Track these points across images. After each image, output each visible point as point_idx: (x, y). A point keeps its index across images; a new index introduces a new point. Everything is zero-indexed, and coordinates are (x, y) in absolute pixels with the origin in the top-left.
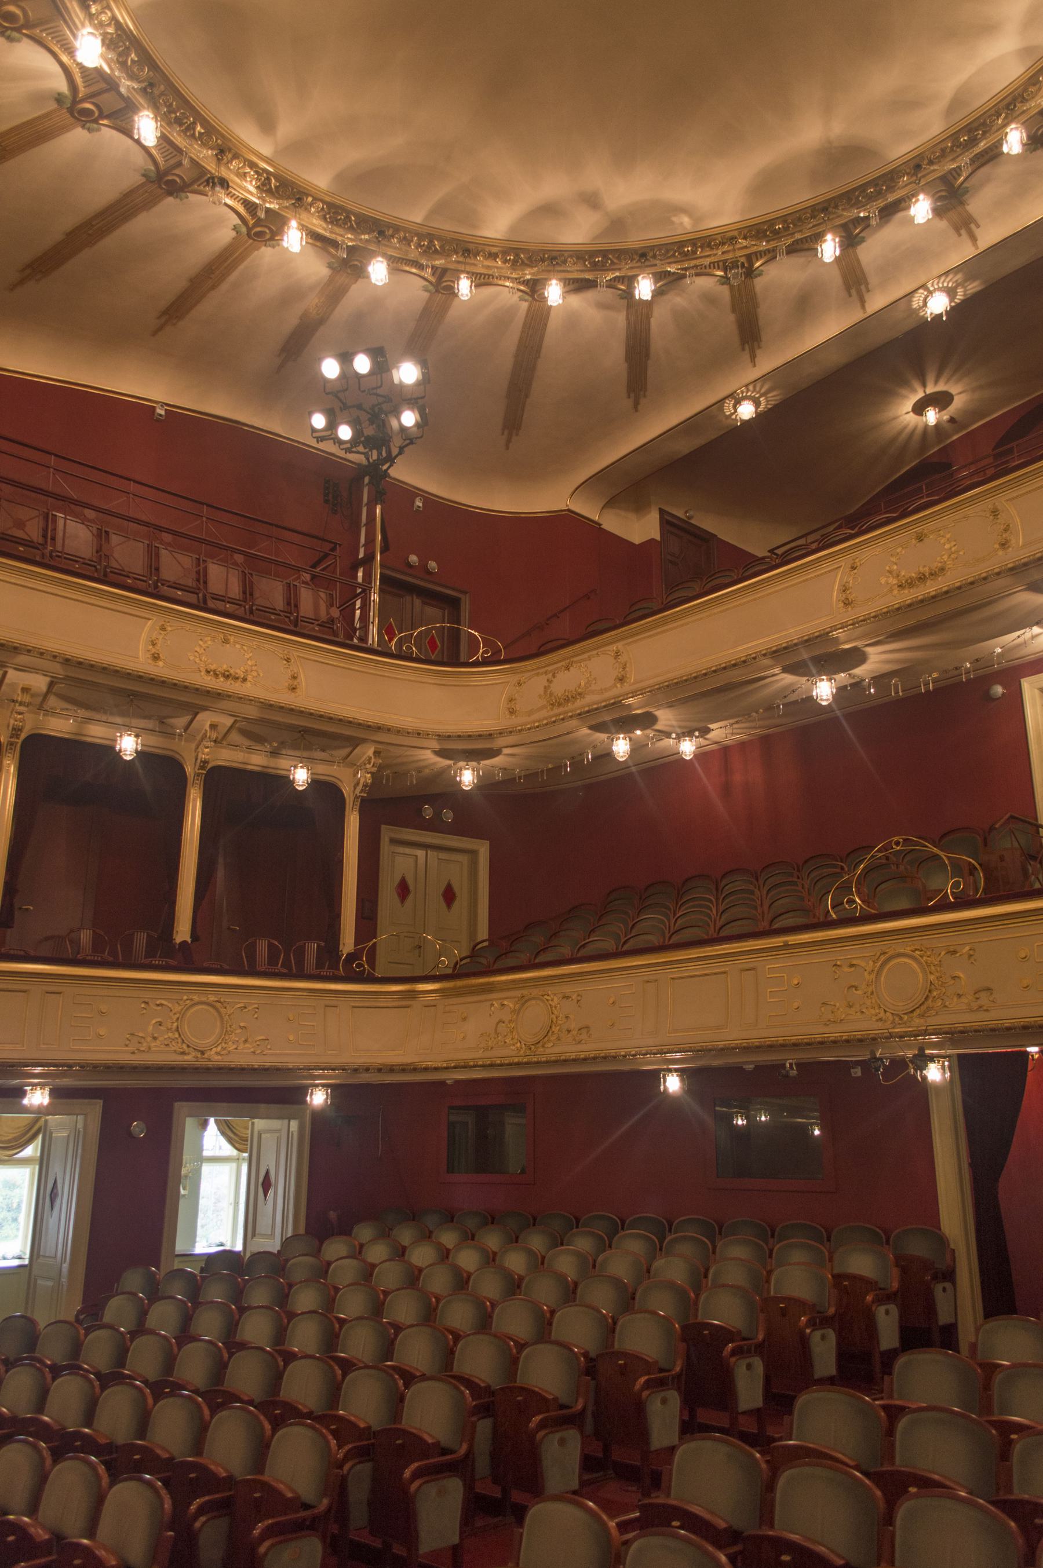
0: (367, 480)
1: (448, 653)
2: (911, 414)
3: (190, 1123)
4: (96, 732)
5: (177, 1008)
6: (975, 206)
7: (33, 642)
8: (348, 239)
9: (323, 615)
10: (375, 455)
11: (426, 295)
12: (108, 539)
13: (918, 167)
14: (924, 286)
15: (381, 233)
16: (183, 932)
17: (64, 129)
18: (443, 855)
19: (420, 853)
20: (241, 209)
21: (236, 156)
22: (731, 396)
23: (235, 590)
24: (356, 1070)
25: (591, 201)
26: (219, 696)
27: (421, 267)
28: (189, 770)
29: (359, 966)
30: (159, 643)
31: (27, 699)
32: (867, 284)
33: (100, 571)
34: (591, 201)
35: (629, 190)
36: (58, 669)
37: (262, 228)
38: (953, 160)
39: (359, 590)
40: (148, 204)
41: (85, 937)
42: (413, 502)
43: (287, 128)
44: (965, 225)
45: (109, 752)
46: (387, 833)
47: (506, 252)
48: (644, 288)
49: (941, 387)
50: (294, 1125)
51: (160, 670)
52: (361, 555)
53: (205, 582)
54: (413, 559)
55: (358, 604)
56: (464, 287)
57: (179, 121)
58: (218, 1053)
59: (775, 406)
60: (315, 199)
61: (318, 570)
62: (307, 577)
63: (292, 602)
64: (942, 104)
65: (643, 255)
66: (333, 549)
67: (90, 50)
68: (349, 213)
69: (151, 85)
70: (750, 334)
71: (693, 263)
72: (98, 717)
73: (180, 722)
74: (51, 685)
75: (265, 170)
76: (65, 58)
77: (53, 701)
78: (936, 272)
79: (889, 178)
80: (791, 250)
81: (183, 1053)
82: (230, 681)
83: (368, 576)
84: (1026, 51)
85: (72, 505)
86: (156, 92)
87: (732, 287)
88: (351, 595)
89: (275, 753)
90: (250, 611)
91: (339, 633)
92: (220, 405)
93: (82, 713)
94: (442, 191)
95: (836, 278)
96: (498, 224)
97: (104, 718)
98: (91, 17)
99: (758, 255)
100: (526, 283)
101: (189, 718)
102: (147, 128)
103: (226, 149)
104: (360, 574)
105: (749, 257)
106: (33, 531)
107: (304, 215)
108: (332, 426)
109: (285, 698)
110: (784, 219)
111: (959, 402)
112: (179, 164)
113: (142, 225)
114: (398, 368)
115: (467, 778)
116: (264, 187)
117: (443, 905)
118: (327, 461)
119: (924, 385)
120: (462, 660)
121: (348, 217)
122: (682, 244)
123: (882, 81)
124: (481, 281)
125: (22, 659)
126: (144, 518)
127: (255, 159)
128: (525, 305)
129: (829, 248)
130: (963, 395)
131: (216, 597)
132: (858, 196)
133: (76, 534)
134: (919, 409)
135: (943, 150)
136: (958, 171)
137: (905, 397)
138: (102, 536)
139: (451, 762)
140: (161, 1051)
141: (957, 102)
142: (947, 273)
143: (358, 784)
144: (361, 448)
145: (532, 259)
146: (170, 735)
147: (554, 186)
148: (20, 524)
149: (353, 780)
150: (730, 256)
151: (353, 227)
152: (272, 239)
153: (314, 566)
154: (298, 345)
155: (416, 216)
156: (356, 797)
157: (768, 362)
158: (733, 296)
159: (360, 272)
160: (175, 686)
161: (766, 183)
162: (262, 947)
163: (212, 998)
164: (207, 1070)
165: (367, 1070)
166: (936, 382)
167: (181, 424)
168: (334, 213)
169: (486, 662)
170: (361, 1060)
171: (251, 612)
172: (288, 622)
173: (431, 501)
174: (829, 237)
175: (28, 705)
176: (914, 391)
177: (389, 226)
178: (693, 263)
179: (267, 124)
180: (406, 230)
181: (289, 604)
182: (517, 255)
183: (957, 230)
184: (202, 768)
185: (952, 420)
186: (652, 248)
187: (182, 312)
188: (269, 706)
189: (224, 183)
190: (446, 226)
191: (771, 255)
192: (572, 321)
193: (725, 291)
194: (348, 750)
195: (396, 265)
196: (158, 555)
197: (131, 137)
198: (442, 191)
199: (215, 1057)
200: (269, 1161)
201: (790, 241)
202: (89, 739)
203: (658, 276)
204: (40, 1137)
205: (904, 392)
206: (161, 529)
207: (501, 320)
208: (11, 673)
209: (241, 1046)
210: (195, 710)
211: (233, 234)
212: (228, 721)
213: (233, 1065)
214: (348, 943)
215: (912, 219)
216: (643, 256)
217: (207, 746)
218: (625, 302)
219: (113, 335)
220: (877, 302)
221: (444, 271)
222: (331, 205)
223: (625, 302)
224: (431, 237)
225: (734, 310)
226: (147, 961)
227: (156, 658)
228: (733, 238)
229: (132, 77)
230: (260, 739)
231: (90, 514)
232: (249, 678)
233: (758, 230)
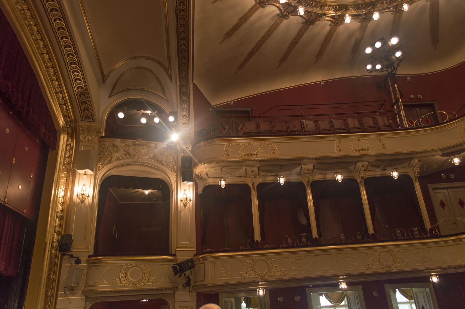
0: (389, 78)
1: (435, 121)
3: (391, 291)
4: (329, 176)
5: (377, 254)
7: (306, 156)
8: (364, 11)
9: (387, 123)
10: (390, 70)
11: (393, 16)
12: (318, 123)
15: (373, 5)
16: (371, 230)
17: (281, 22)
18: (454, 190)
19: (445, 191)
20: (330, 19)
21: (325, 6)
23: (357, 125)
24: (446, 268)
26: (362, 156)
28: (358, 181)
29: (435, 232)
30: (340, 146)
31: (309, 172)
33: (318, 131)
36: (315, 161)
37: (338, 20)
39: (396, 112)
41: (342, 236)
42: (407, 79)
45: (336, 181)
46: (430, 187)
50: (428, 289)
51: (342, 154)
52: (394, 101)
53: (348, 125)
54: (412, 96)
55: (397, 116)
57: (308, 5)
58: (394, 267)
61: (381, 110)
62: (378, 114)
63: (376, 123)
66: (385, 102)
72: (328, 172)
73: (352, 168)
74: (314, 166)
75: (335, 5)
76: (277, 5)
77: (315, 171)
81: (383, 268)
82: (364, 151)
83: (398, 107)
85: (305, 117)
88: (394, 115)
89: (384, 170)
90: (363, 129)
91: (394, 126)
92: (338, 75)
93: (324, 172)
97: (330, 172)
101: (354, 165)
104: (395, 107)
106: (299, 127)
107: (349, 12)
108: (374, 67)
109: (383, 152)
112: (311, 15)
113: (306, 36)
114: (390, 41)
115: (456, 161)
116: (336, 10)
117: (460, 207)
118: (375, 77)
120: (440, 122)
121: (362, 6)
125: (305, 161)
126: (326, 113)
127: (331, 4)
131: (352, 129)
133: (309, 124)
138: (316, 122)
139: (448, 157)
140: (376, 269)
143: (415, 172)
144: (385, 69)
146: (351, 172)
148: (295, 126)
149: (413, 172)
152: (341, 22)
153: (379, 110)
154: (357, 47)
156: (416, 177)
159: (371, 18)
160: (348, 157)
162: (398, 231)
163: (387, 250)
164: (393, 273)
165: (450, 268)
167: (328, 84)
169: (451, 120)
170: (446, 265)
171: (364, 129)
172: (377, 128)
173: (412, 77)
175: (309, 173)
181: (375, 123)
184: (362, 179)
187: (323, 53)
188: (378, 155)
189: (324, 14)
194: (408, 163)
196: (332, 122)
199: (394, 268)
200: (422, 302)
202: (328, 179)
204: (346, 298)
206: (331, 115)
208: (303, 166)
209: (402, 264)
210: (356, 163)
212: (367, 163)
213: (401, 271)
214: (428, 226)
217: (362, 173)
219: (306, 69)
221: (397, 6)
222: (355, 5)
226: (363, 241)
227: (340, 151)
230: (378, 166)
231: (311, 117)
232: (369, 149)
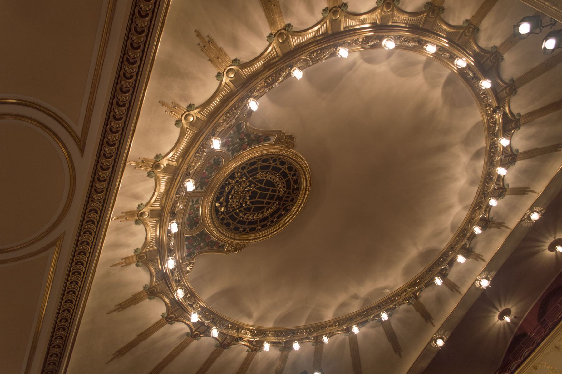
2: (501, 320)
6: (477, 250)
8: (284, 339)
11: (314, 347)
13: (452, 248)
14: (476, 280)
15: (293, 333)
17: (190, 342)
20: (248, 344)
21: (243, 329)
22: (432, 339)
25: (355, 297)
27: (309, 339)
32: (457, 286)
34: (355, 297)
35: (365, 289)
37: (256, 347)
38: (462, 242)
40: (221, 353)
43: (255, 315)
44: (478, 257)
47: (335, 323)
48: (385, 317)
49: (504, 308)
56: (326, 339)
59: (450, 337)
60: (270, 331)
64: (449, 229)
65: (379, 306)
67: (195, 318)
68: (281, 331)
69: (214, 319)
70: (427, 317)
71: (396, 302)
76: (188, 322)
78: (478, 274)
79: (445, 255)
80: (427, 286)
84: (465, 208)
86: (215, 320)
87: (413, 305)
94: (308, 313)
95: (446, 289)
96: (329, 315)
98: (193, 308)
99: (416, 292)
100: (345, 330)
102: (215, 332)
103: (239, 328)
105: (413, 293)
110: (419, 278)
111: (514, 310)
112: (226, 338)
116: (254, 334)
119: (497, 310)
122: (390, 298)
123: (427, 231)
124: (330, 335)
128: (348, 337)
129: (438, 281)
130: (514, 308)
132: (440, 262)
134: (501, 317)
135: (457, 241)
136: (465, 244)
137: (494, 316)
141: (453, 227)
142: (481, 273)
145: (344, 322)
147: (342, 297)
150: (407, 295)
151: (284, 335)
152: (260, 349)
155: (303, 323)
157: (438, 324)
158: (415, 307)
159: (290, 348)
161: (407, 271)
166: (501, 307)
168: (277, 333)
174: (436, 278)
176: (495, 313)
177: (295, 330)
178: (396, 302)
179: (249, 316)
180: (300, 329)
182: (339, 322)
183: (476, 259)
185: (515, 317)
186: (381, 303)
189: (241, 339)
190: (313, 323)
191: (421, 290)
192: (365, 335)
193: (411, 307)
195: (301, 342)
197: (210, 336)
198: (308, 313)
201: (424, 284)
203: (386, 311)
205: (492, 314)
207: (342, 344)
211: (247, 353)
215: (460, 263)
216: (380, 307)
218: (380, 323)
220: (464, 290)
221: (317, 337)
222: (274, 331)
223: (380, 323)
224: (309, 328)
225: (417, 311)
228: (405, 290)
229: (207, 319)
233: (413, 284)
